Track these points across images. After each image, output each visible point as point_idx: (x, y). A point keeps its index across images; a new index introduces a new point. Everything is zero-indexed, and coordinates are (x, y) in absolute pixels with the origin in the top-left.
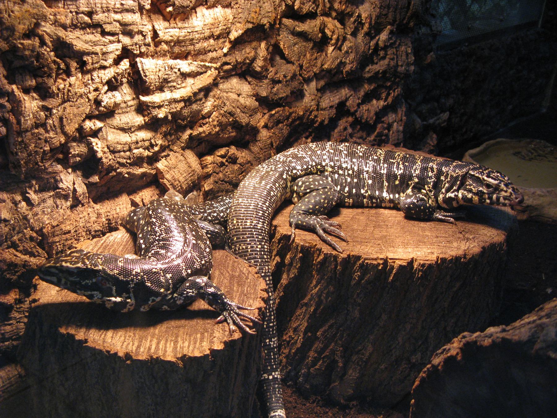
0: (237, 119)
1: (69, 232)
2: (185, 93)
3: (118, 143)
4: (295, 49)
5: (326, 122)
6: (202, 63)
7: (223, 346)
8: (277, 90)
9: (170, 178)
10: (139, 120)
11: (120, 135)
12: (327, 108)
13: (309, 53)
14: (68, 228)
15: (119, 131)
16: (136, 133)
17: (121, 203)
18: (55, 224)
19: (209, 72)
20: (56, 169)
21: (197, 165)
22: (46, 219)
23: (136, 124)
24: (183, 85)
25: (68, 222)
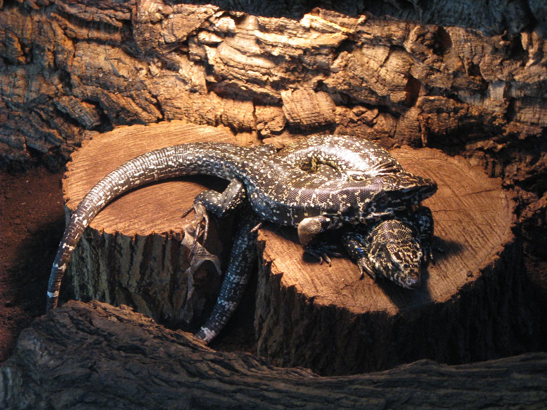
0: (371, 87)
1: (179, 108)
2: (302, 43)
3: (231, 59)
4: (466, 46)
5: (522, 137)
6: (330, 24)
7: (440, 300)
8: (435, 78)
9: (288, 109)
10: (256, 49)
11: (236, 54)
12: (527, 122)
13: (488, 56)
14: (179, 105)
15: (236, 51)
16: (252, 58)
17: (243, 107)
18: (168, 97)
19: (337, 34)
20: (174, 58)
21: (329, 110)
22: (162, 90)
23: (252, 52)
24: (305, 36)
25: (179, 101)
